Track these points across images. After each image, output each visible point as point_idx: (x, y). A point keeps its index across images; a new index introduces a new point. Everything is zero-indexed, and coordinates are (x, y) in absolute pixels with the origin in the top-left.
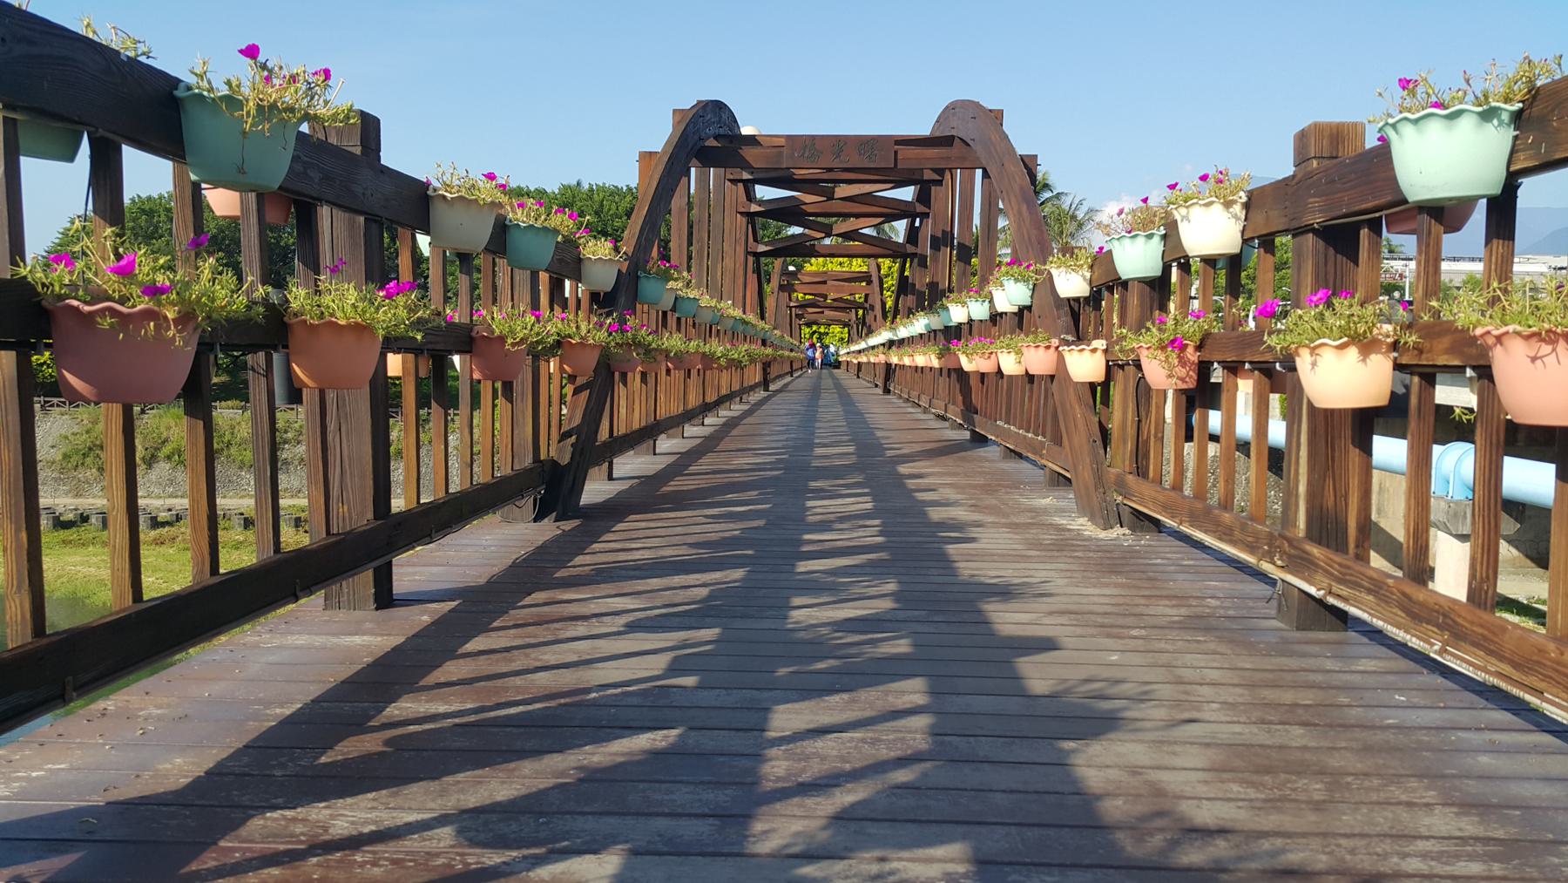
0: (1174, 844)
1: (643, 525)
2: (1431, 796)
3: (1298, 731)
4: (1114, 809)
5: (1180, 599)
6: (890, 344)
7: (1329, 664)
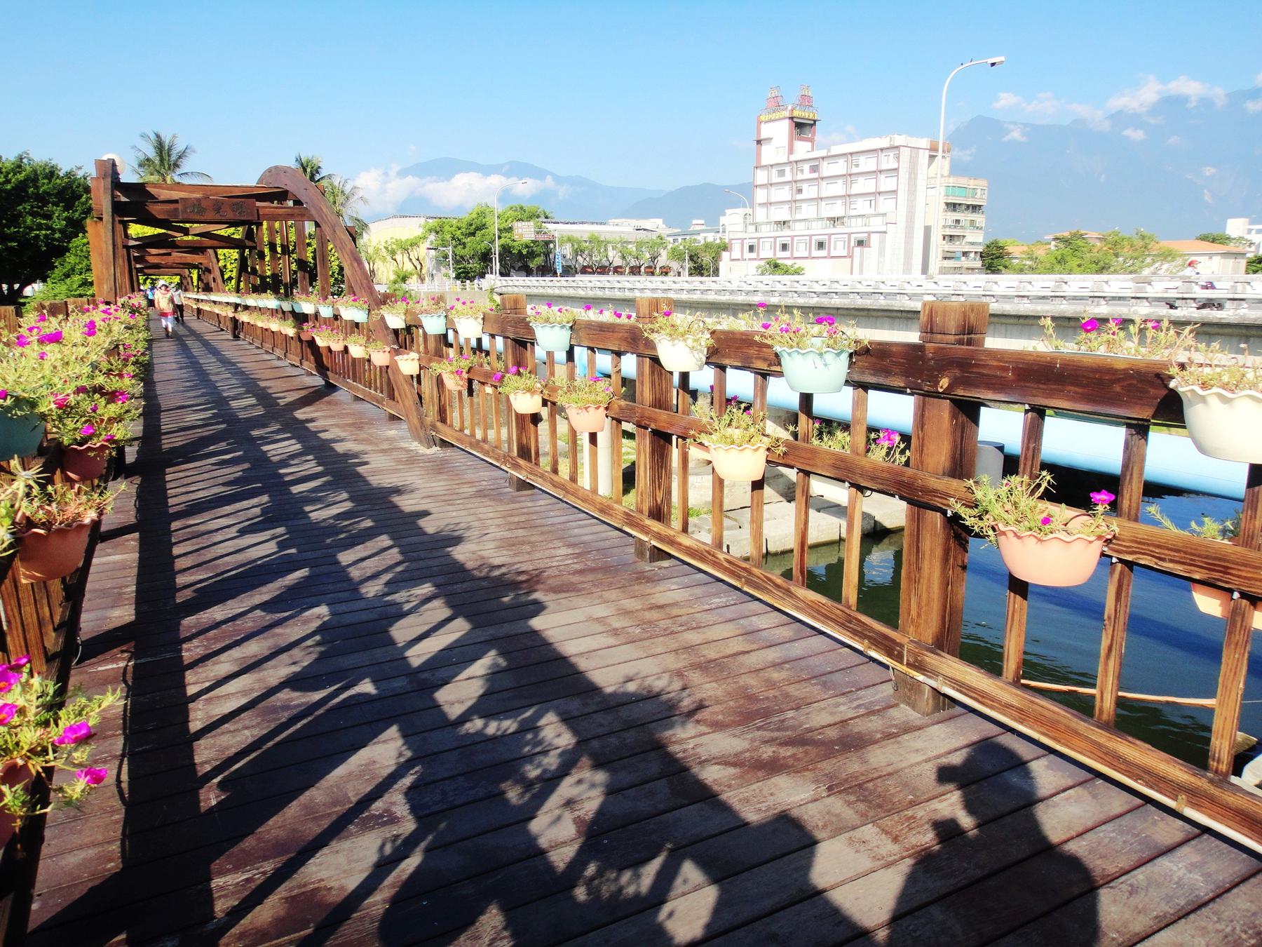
0: (490, 571)
1: (181, 475)
2: (560, 544)
3: (520, 531)
4: (470, 565)
5: (471, 483)
6: (236, 306)
7: (529, 504)
